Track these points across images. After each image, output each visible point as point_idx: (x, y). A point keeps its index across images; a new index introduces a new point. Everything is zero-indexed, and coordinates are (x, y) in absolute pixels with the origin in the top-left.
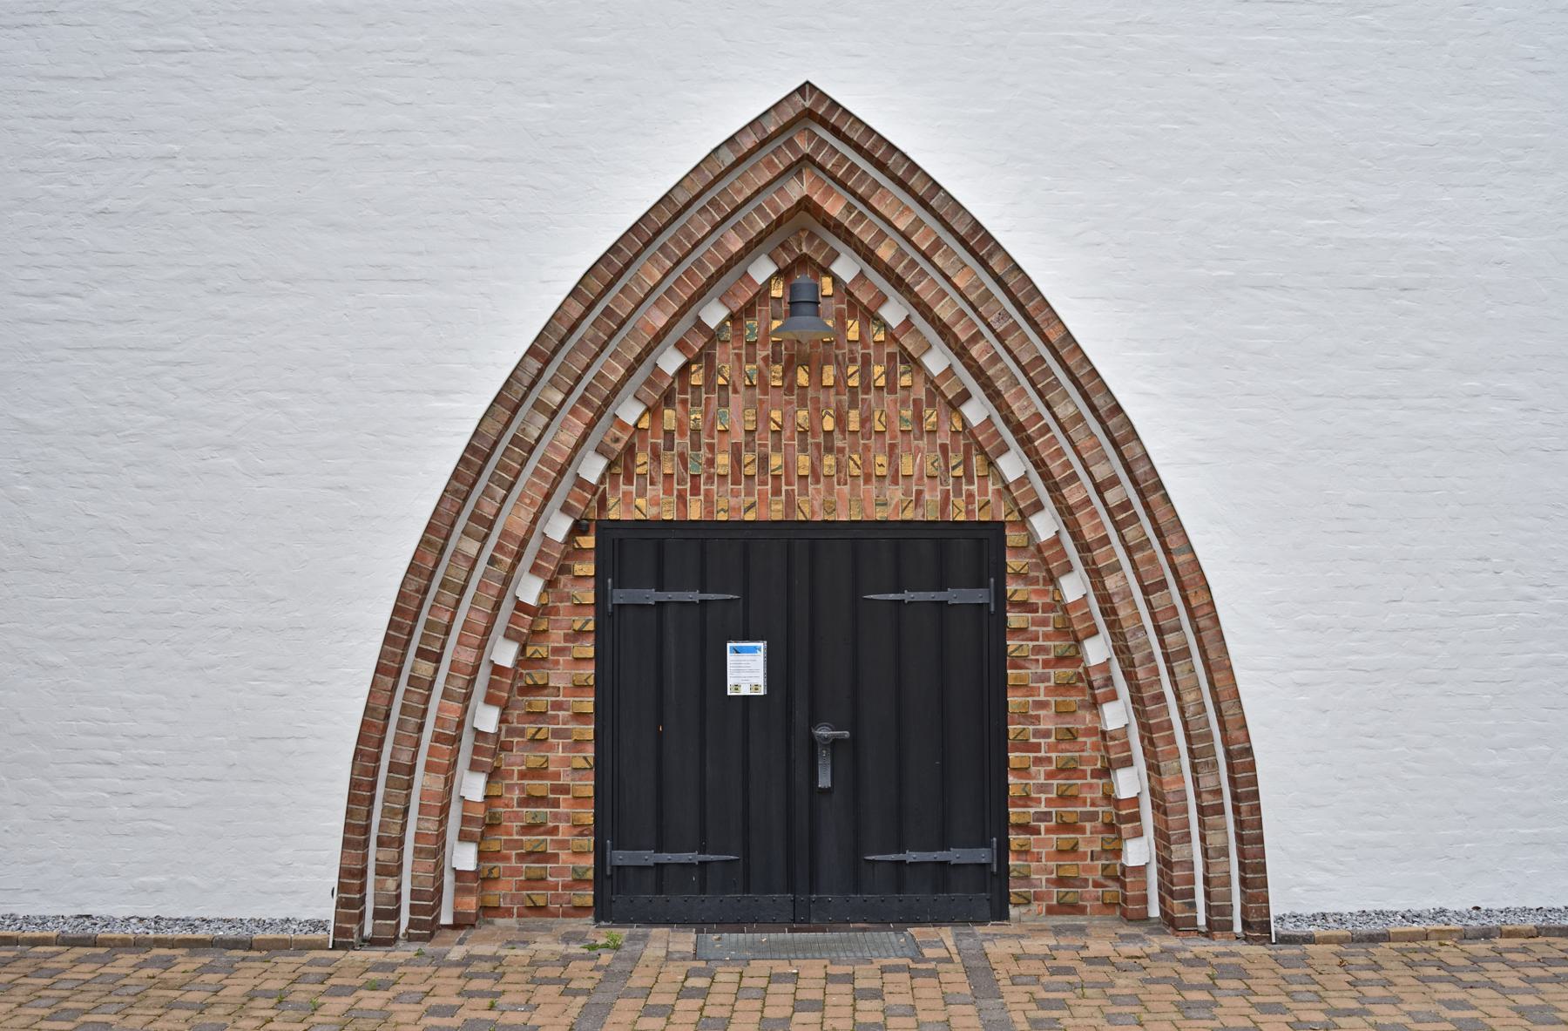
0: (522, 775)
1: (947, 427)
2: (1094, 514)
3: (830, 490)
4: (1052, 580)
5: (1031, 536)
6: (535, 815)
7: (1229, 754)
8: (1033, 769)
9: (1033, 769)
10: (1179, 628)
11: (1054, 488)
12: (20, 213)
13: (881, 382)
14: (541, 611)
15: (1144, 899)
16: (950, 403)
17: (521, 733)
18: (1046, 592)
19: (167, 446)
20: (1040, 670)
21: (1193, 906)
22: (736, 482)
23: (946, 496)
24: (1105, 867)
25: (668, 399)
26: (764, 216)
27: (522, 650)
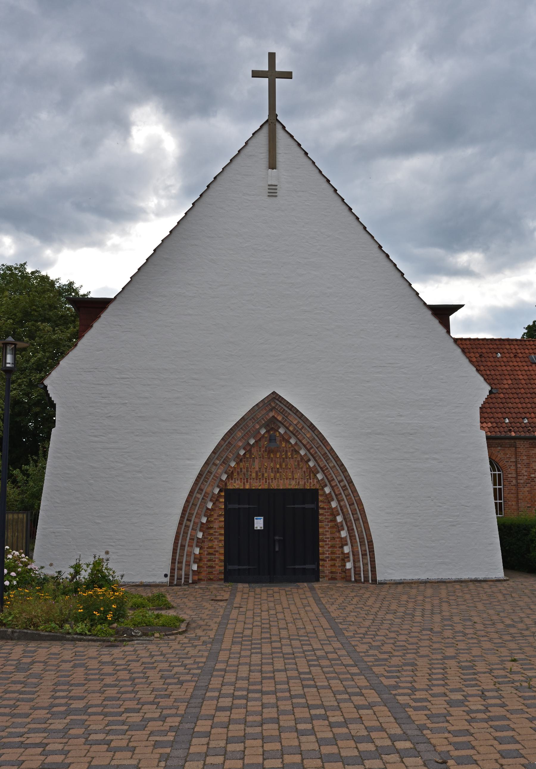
0: (207, 548)
1: (305, 467)
2: (338, 488)
3: (278, 482)
4: (329, 502)
5: (325, 492)
6: (210, 557)
7: (368, 542)
8: (325, 546)
9: (325, 546)
10: (357, 514)
11: (329, 482)
12: (90, 416)
13: (290, 456)
14: (212, 510)
15: (350, 576)
16: (306, 462)
17: (207, 538)
18: (328, 505)
19: (126, 472)
20: (327, 523)
21: (360, 577)
22: (257, 480)
23: (305, 483)
24: (342, 569)
25: (241, 460)
26: (264, 420)
27: (207, 519)
